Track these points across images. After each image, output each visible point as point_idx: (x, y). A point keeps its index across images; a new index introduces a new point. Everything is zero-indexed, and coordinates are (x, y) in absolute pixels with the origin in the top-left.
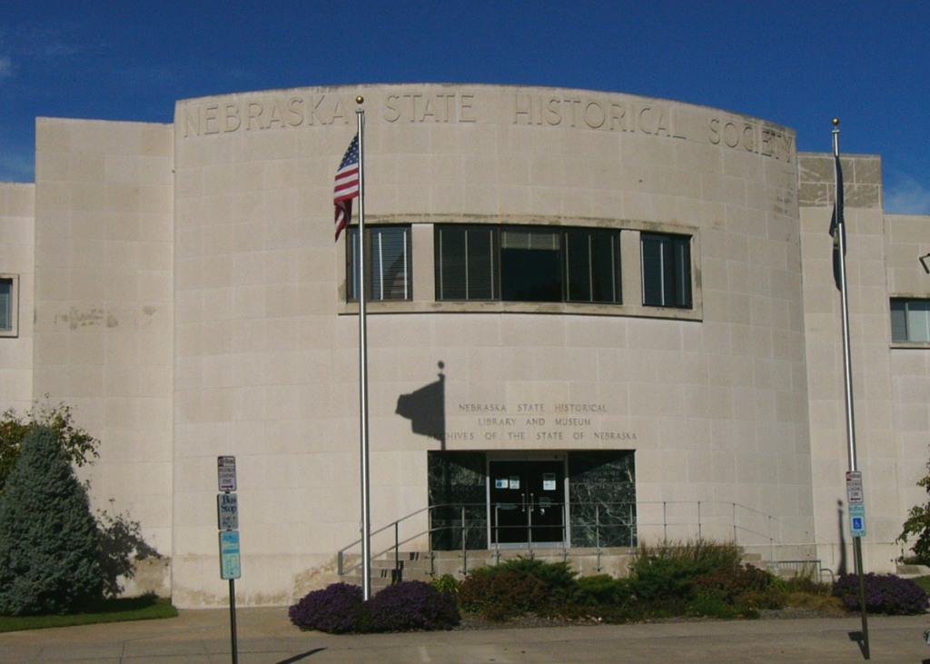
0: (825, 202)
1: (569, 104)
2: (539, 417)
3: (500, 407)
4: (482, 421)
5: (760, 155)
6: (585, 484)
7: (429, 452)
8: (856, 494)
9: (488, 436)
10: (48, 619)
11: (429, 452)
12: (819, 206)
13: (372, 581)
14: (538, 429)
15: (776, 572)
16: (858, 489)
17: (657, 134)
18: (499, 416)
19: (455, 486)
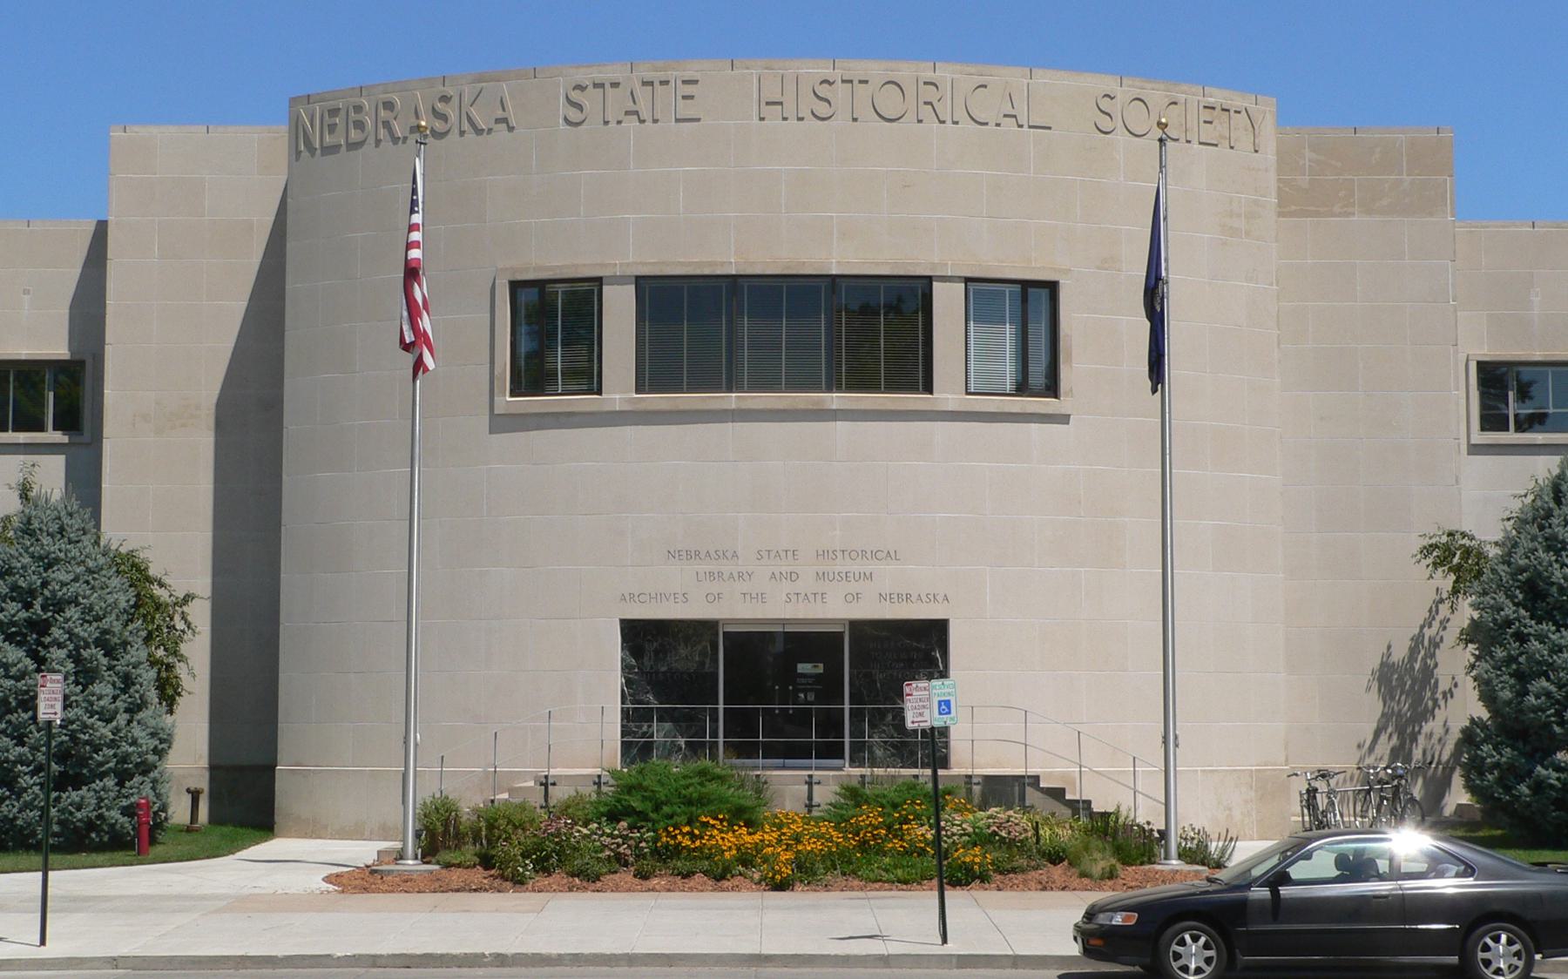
0: (1350, 210)
1: (127, 128)
2: (789, 569)
3: (729, 555)
4: (701, 576)
5: (1196, 146)
6: (873, 672)
7: (623, 622)
8: (921, 714)
9: (711, 598)
10: (119, 855)
11: (623, 622)
12: (1339, 215)
13: (401, 829)
14: (787, 587)
15: (1413, 825)
16: (924, 707)
17: (998, 125)
18: (727, 568)
19: (664, 673)
